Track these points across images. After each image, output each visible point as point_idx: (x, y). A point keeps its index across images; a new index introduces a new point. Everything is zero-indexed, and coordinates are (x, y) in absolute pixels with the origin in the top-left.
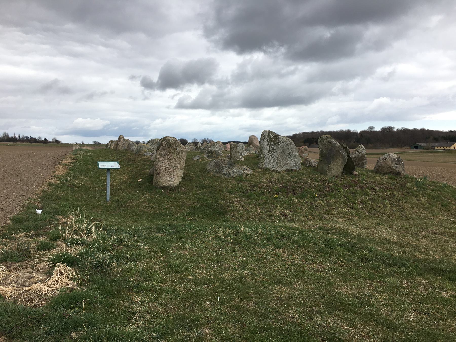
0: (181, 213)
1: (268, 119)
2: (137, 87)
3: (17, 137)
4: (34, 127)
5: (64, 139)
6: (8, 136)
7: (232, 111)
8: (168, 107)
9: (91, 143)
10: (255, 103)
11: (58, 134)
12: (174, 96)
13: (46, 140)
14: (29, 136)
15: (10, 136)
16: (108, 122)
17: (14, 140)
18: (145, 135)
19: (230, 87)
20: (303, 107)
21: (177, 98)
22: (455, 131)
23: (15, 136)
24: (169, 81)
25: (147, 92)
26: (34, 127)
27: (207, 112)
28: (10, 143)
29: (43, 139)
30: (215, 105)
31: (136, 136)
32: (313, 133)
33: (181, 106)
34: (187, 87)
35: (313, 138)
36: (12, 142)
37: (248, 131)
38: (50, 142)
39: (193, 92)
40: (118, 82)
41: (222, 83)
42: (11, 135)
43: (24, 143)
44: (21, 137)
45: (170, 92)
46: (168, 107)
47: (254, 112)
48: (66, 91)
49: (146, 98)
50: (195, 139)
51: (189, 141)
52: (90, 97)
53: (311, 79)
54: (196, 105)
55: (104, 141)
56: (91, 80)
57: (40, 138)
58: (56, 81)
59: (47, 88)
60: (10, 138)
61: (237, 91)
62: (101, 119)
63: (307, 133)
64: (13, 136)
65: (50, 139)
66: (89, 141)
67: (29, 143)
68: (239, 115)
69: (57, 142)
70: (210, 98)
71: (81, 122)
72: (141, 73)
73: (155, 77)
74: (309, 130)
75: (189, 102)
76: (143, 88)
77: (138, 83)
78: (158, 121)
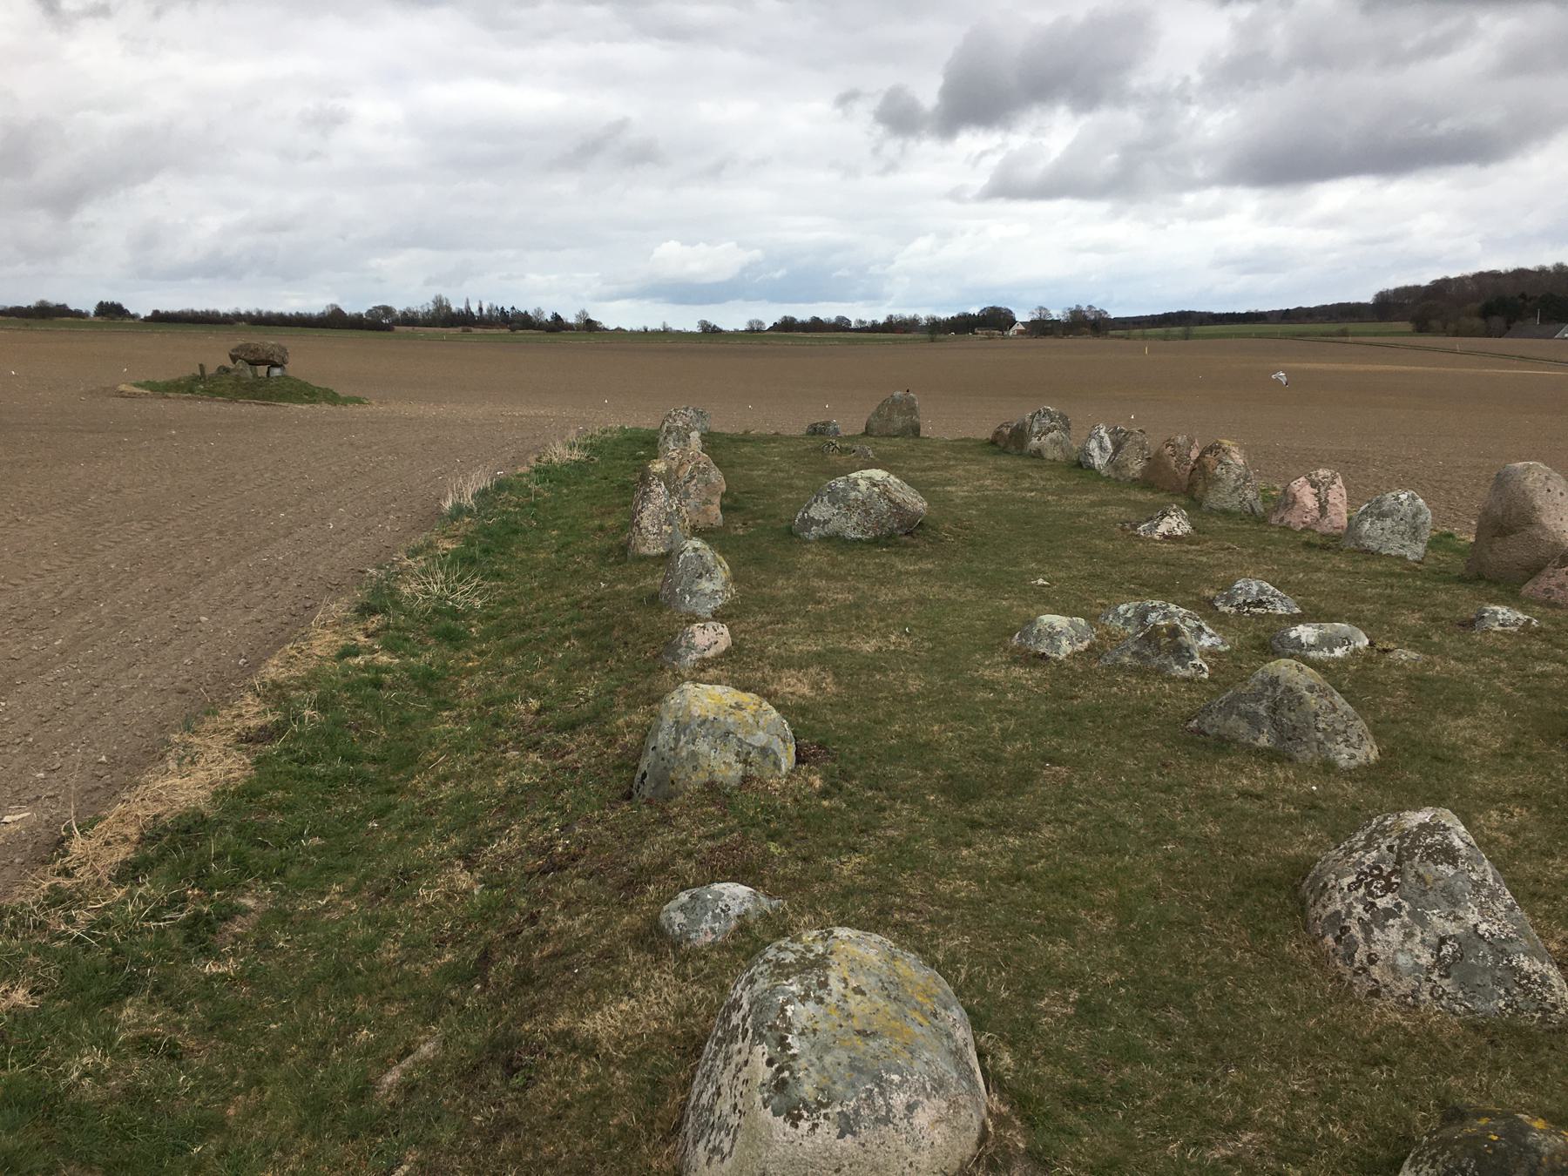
0: (544, 623)
1: (1331, 221)
2: (860, 128)
3: (474, 309)
4: (534, 278)
5: (612, 316)
6: (449, 308)
7: (1189, 199)
8: (956, 195)
9: (694, 327)
10: (1284, 164)
11: (600, 298)
12: (983, 154)
13: (557, 318)
14: (507, 309)
15: (454, 308)
16: (757, 254)
17: (465, 320)
18: (873, 297)
19: (1193, 111)
20: (1469, 171)
21: (994, 161)
22: (1560, 268)
23: (468, 308)
24: (978, 99)
25: (892, 146)
26: (534, 278)
27: (1102, 207)
28: (452, 331)
29: (548, 317)
30: (1121, 183)
31: (810, 300)
32: (1520, 274)
33: (1007, 188)
34: (1034, 116)
35: (1523, 296)
36: (460, 329)
37: (1246, 272)
38: (569, 327)
39: (1053, 135)
40: (806, 115)
41: (1162, 102)
42: (457, 306)
43: (494, 331)
44: (485, 311)
45: (971, 141)
46: (956, 195)
47: (1277, 198)
48: (643, 156)
49: (891, 167)
50: (1041, 308)
51: (1022, 316)
52: (716, 172)
53: (1520, 62)
54: (1061, 185)
55: (732, 319)
56: (726, 113)
57: (539, 312)
58: (622, 125)
59: (590, 150)
60: (454, 315)
61: (1216, 124)
62: (739, 245)
63: (1494, 275)
64: (463, 307)
65: (570, 317)
66: (686, 320)
67: (506, 331)
68: (1217, 212)
69: (590, 326)
70: (1113, 157)
71: (676, 257)
72: (879, 80)
73: (928, 93)
74: (1503, 262)
75: (1036, 171)
76: (880, 130)
77: (863, 111)
78: (923, 244)
